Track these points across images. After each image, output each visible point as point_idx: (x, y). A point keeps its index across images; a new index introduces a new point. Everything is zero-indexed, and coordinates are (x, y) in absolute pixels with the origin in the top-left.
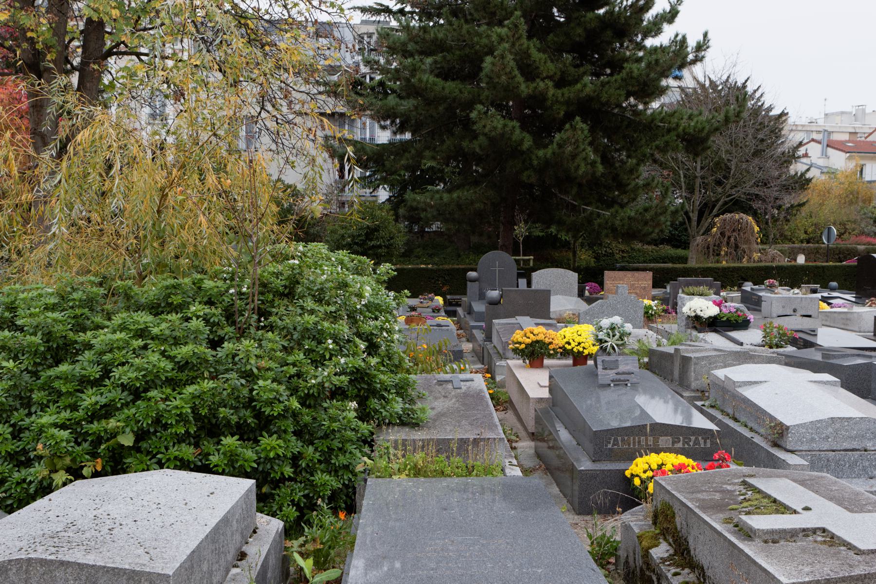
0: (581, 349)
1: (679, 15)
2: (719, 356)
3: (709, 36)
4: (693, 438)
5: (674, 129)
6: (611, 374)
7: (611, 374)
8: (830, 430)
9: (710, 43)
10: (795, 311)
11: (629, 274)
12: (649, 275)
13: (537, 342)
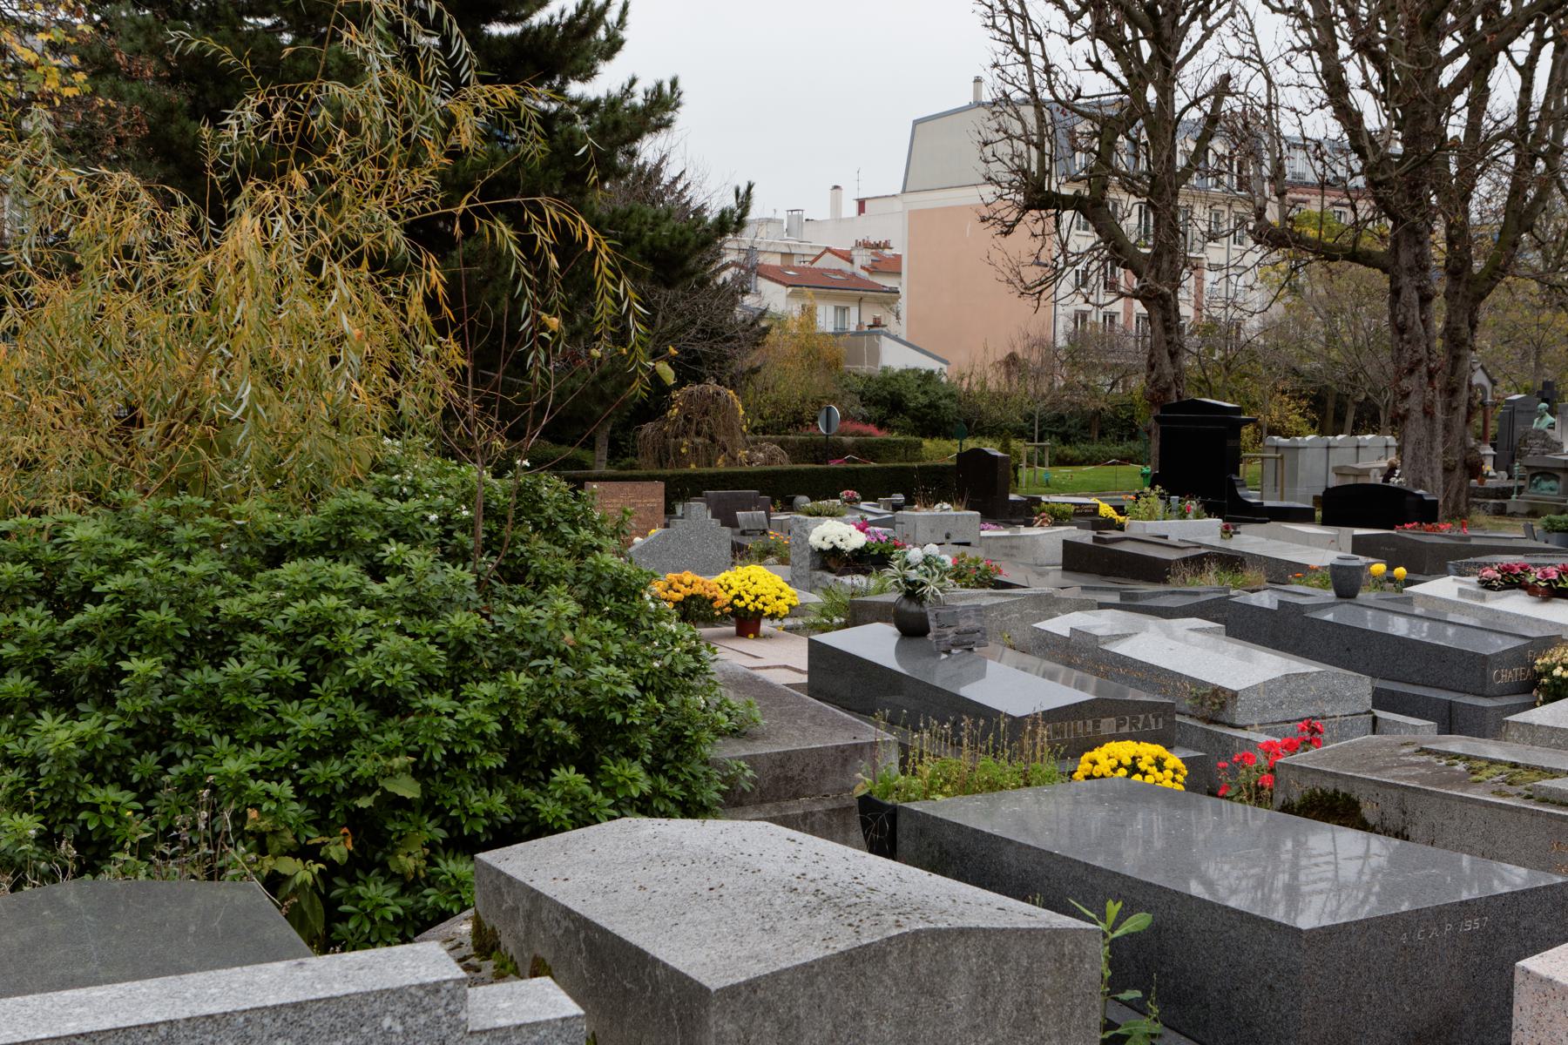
0: (760, 606)
1: (624, 47)
2: (1013, 603)
3: (681, 85)
4: (1142, 717)
5: (634, 241)
8: (1285, 692)
9: (682, 99)
10: (948, 537)
11: (627, 486)
12: (660, 487)
13: (693, 597)
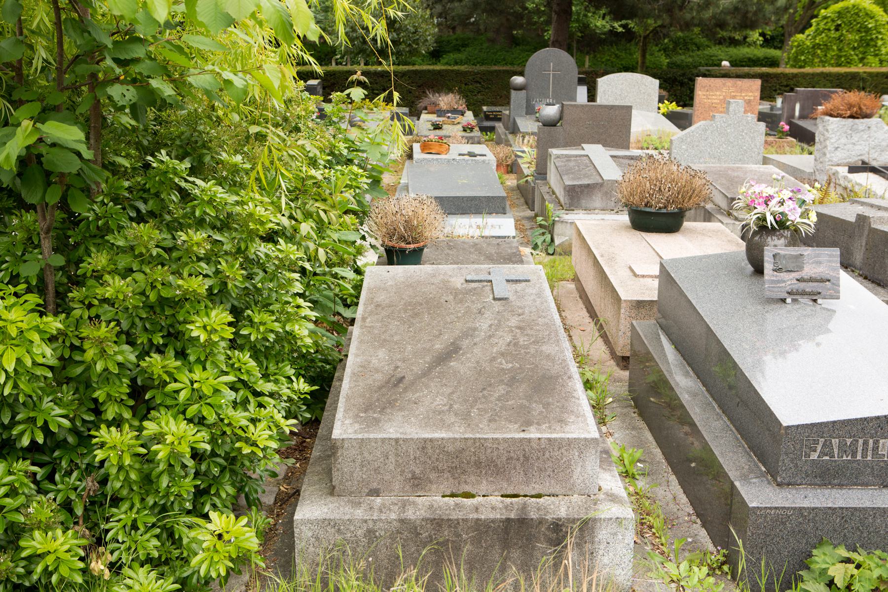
6: (789, 280)
7: (789, 280)
12: (758, 83)
